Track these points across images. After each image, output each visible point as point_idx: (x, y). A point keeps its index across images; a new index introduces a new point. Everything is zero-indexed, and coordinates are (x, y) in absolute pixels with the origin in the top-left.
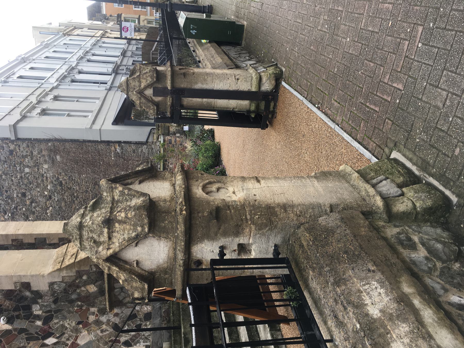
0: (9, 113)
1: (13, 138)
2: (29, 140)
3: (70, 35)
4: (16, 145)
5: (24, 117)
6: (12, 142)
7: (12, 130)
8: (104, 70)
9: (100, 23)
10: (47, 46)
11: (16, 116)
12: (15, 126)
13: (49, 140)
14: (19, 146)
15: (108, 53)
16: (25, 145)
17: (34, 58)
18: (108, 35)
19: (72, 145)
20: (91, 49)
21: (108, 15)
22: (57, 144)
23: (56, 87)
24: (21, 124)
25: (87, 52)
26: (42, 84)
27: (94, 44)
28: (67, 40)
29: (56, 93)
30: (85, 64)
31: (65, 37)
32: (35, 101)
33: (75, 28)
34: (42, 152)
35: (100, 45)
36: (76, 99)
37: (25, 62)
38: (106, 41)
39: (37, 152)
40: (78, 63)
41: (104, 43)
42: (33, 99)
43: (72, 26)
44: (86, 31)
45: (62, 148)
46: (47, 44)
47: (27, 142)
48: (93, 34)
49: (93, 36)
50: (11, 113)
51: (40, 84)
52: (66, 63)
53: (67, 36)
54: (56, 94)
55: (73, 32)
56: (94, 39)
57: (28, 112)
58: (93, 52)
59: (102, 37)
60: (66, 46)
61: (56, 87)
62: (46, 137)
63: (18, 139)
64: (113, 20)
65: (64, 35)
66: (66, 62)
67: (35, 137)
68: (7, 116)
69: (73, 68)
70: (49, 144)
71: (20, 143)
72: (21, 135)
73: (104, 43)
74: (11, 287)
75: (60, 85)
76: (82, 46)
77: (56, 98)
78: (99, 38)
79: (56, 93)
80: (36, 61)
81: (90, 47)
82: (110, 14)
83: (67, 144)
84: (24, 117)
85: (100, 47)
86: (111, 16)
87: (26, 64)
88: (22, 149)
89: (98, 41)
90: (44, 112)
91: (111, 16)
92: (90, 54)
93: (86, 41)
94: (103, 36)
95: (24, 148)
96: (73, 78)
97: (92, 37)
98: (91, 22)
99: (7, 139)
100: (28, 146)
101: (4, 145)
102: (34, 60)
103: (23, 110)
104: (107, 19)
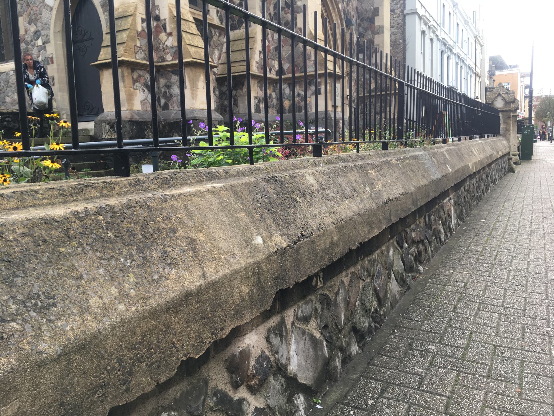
0: (422, 6)
1: (405, 12)
2: (404, 25)
3: (476, 42)
4: (399, 14)
5: (420, 18)
6: (403, 11)
7: (413, 11)
8: (450, 80)
9: (488, 69)
10: (466, 22)
11: (421, 12)
12: (416, 13)
13: (404, 40)
14: (398, 17)
15: (463, 80)
16: (399, 21)
17: (458, 14)
18: (477, 79)
19: (401, 58)
20: (465, 64)
21: (494, 78)
22: (401, 46)
23: (438, 39)
24: (417, 18)
25: (463, 61)
26: (440, 26)
27: (446, 44)
28: (472, 40)
29: (435, 40)
30: (454, 61)
31: (474, 38)
32: (430, 24)
33: (481, 46)
34: (394, 35)
35: (459, 63)
36: (422, 52)
37: (454, 6)
38: (472, 78)
39: (394, 31)
40: (455, 54)
41: (471, 76)
42: (432, 23)
43: (484, 43)
44: (479, 57)
45: (397, 50)
46: (468, 22)
47: (403, 23)
48: (477, 64)
49: (476, 65)
50: (423, 7)
51: (439, 25)
52: (454, 44)
53: (475, 39)
54: (434, 40)
55: (478, 45)
56: (474, 66)
57: (424, 21)
58: (464, 66)
59: (475, 73)
60: (467, 40)
61: (438, 39)
62: (407, 38)
63: (404, 16)
64: (490, 83)
65: (476, 37)
66: (455, 43)
67: (406, 29)
68: (420, 4)
69: (451, 50)
70: (401, 41)
71: (401, 17)
72: (408, 18)
73: (471, 76)
74: (376, 43)
75: (440, 41)
76: (457, 44)
77: (431, 40)
78: (474, 71)
79: (435, 40)
80: (455, 15)
81: (467, 64)
82: (495, 80)
83: (401, 54)
84: (420, 18)
85: (457, 63)
86: (494, 81)
87: (453, 7)
88: (396, 19)
89: (473, 70)
90: (423, 32)
91: (494, 81)
92: (462, 64)
93: (450, 33)
94: (476, 75)
95: (397, 21)
96: (444, 52)
97: (475, 64)
98: (488, 61)
99: (404, 7)
100: (398, 24)
101: (399, 5)
102: (456, 14)
103: (425, 16)
104: (491, 77)
